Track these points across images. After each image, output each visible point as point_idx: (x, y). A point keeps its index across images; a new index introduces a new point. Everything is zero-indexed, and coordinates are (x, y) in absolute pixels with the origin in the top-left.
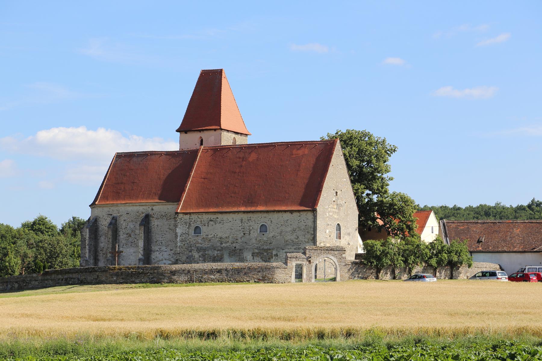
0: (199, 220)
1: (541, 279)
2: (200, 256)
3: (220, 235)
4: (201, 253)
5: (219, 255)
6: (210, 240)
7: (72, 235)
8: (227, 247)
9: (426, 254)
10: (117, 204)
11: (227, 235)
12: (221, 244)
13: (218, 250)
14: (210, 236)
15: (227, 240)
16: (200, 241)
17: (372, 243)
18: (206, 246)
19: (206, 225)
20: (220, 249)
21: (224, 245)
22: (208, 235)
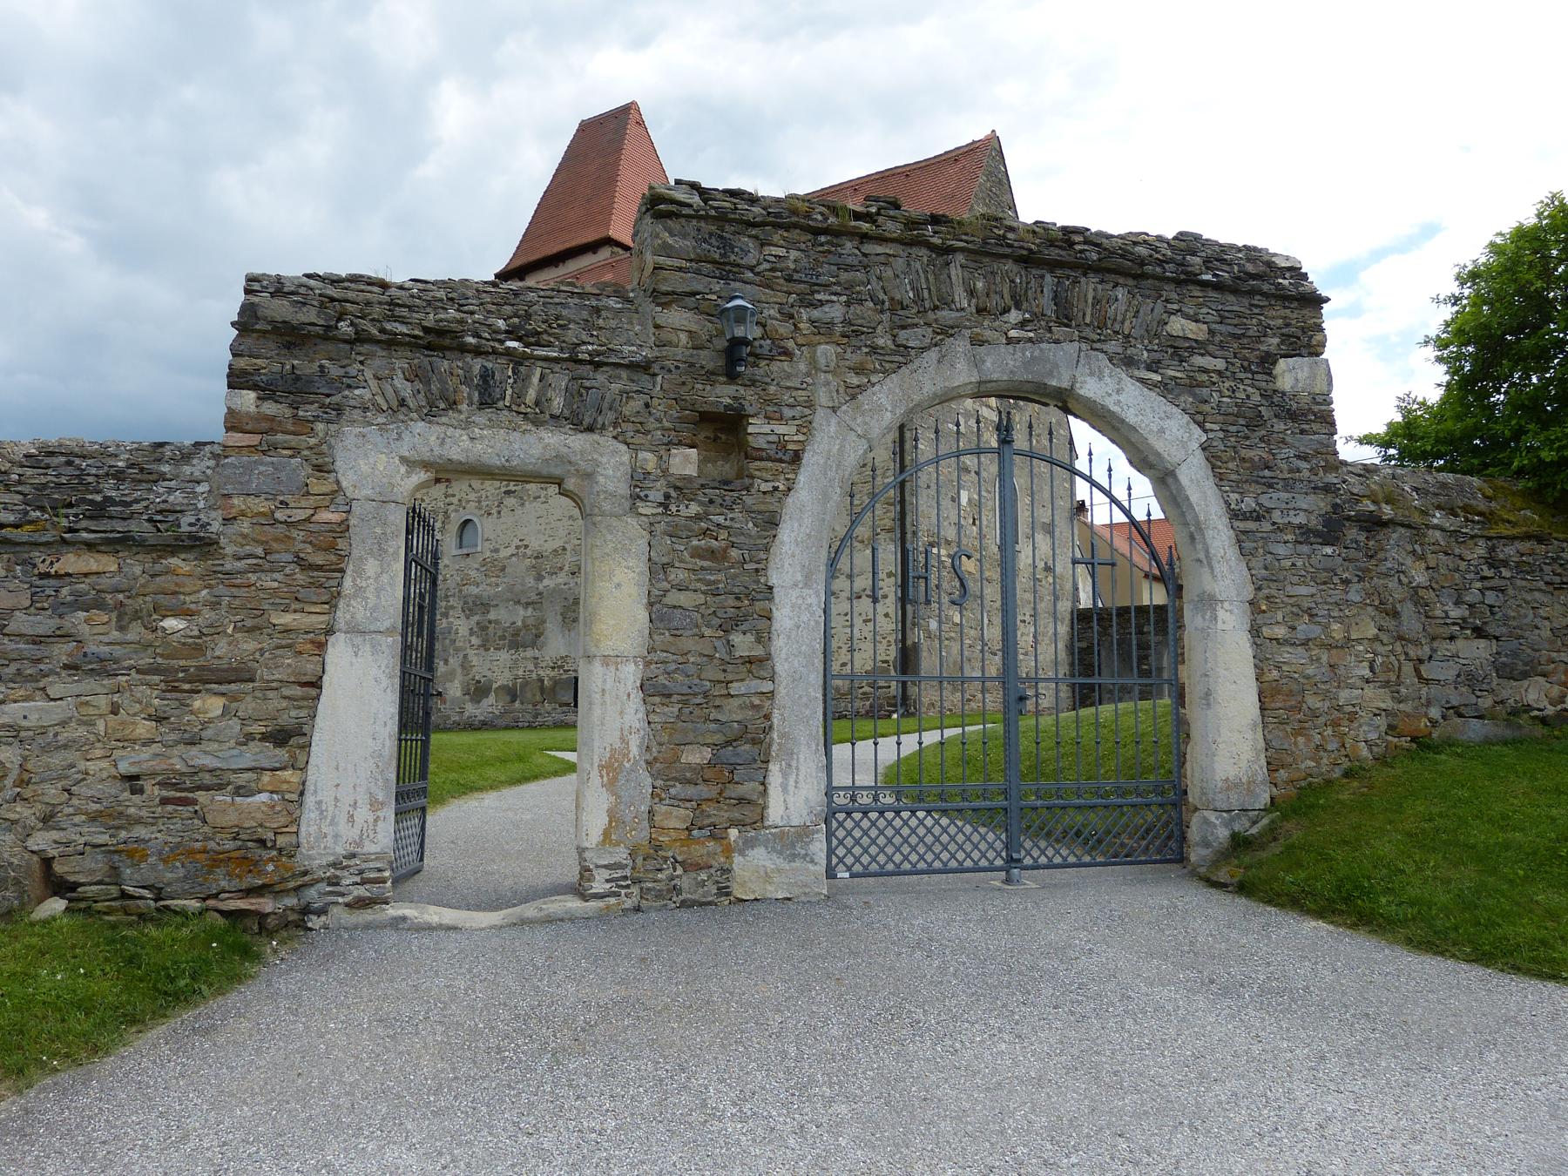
0: (472, 496)
1: (74, 506)
2: (472, 632)
3: (535, 544)
4: (476, 618)
5: (530, 622)
6: (503, 569)
7: (205, 556)
8: (556, 591)
9: (1470, 679)
10: (1139, 647)
11: (557, 544)
12: (540, 578)
13: (528, 604)
14: (504, 553)
15: (558, 561)
16: (473, 573)
17: (880, 408)
18: (491, 591)
19: (494, 511)
20: (534, 598)
21: (546, 582)
22: (496, 551)
